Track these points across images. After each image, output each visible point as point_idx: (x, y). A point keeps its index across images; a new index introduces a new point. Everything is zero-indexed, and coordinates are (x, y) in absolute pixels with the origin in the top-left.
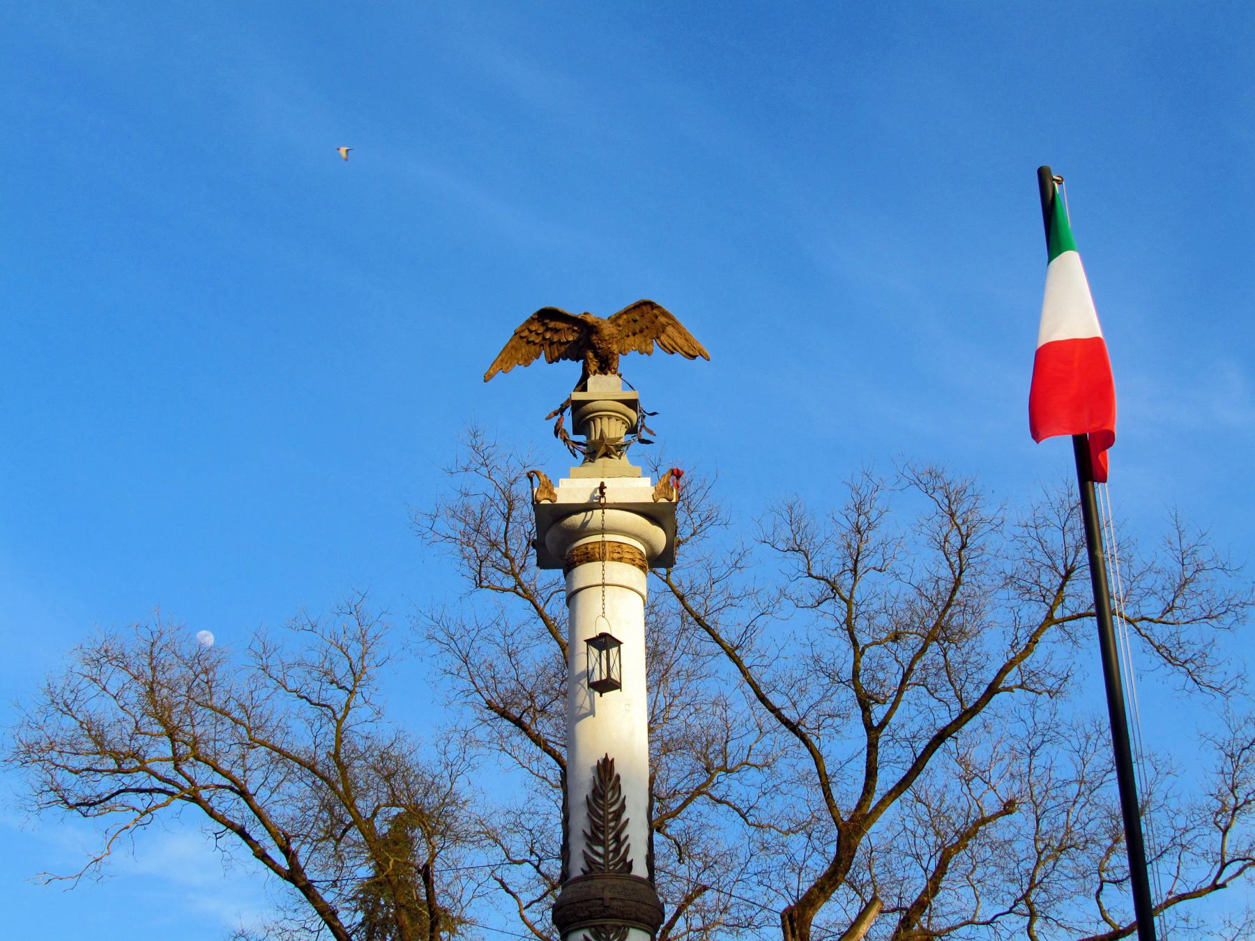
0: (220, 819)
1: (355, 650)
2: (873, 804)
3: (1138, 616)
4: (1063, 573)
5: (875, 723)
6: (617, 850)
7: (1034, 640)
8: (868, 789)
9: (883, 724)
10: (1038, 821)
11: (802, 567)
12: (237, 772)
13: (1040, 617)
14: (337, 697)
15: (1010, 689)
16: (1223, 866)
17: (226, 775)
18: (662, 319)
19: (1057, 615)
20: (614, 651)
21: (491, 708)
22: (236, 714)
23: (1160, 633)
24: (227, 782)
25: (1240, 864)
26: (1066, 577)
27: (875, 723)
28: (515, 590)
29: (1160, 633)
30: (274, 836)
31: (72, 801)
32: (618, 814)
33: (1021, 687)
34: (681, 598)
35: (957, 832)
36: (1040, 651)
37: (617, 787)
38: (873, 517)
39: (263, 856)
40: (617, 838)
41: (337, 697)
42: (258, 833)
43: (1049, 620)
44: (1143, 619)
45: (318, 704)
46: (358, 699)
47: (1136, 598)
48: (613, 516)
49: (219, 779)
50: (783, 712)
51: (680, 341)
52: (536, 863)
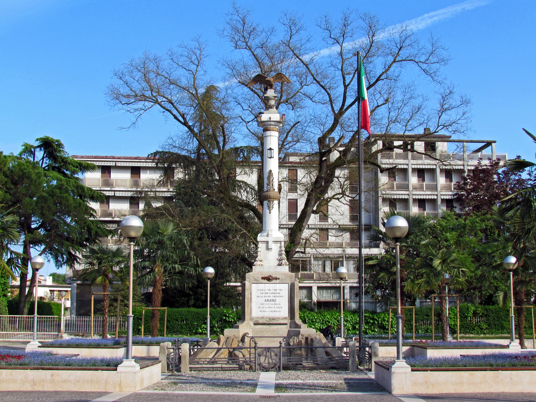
0: (164, 108)
1: (198, 52)
2: (345, 108)
3: (419, 61)
4: (399, 48)
5: (347, 84)
6: (272, 187)
7: (390, 67)
8: (343, 105)
9: (348, 85)
10: (389, 113)
11: (328, 34)
12: (169, 97)
13: (392, 60)
14: (193, 67)
15: (383, 80)
16: (438, 127)
17: (167, 98)
18: (283, 76)
19: (397, 59)
20: (272, 151)
21: (239, 83)
22: (166, 76)
23: (424, 66)
24: (166, 100)
25: (442, 127)
26: (400, 49)
27: (347, 84)
28: (246, 48)
29: (424, 66)
30: (181, 115)
31: (123, 103)
32: (272, 180)
33: (386, 78)
34: (293, 51)
35: (339, 188)
36: (392, 69)
37: (272, 176)
38: (349, 23)
39: (176, 118)
40: (272, 185)
41: (193, 67)
42: (175, 112)
43: (394, 61)
44: (420, 62)
45: (188, 70)
46: (199, 68)
47: (419, 56)
48: (272, 123)
49: (164, 99)
50: (321, 83)
51: (286, 80)
52: (251, 110)
